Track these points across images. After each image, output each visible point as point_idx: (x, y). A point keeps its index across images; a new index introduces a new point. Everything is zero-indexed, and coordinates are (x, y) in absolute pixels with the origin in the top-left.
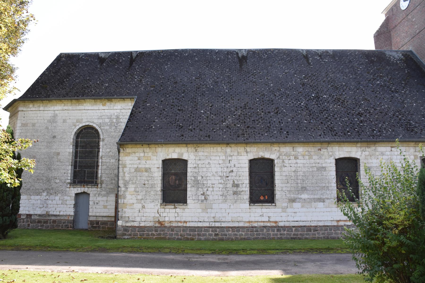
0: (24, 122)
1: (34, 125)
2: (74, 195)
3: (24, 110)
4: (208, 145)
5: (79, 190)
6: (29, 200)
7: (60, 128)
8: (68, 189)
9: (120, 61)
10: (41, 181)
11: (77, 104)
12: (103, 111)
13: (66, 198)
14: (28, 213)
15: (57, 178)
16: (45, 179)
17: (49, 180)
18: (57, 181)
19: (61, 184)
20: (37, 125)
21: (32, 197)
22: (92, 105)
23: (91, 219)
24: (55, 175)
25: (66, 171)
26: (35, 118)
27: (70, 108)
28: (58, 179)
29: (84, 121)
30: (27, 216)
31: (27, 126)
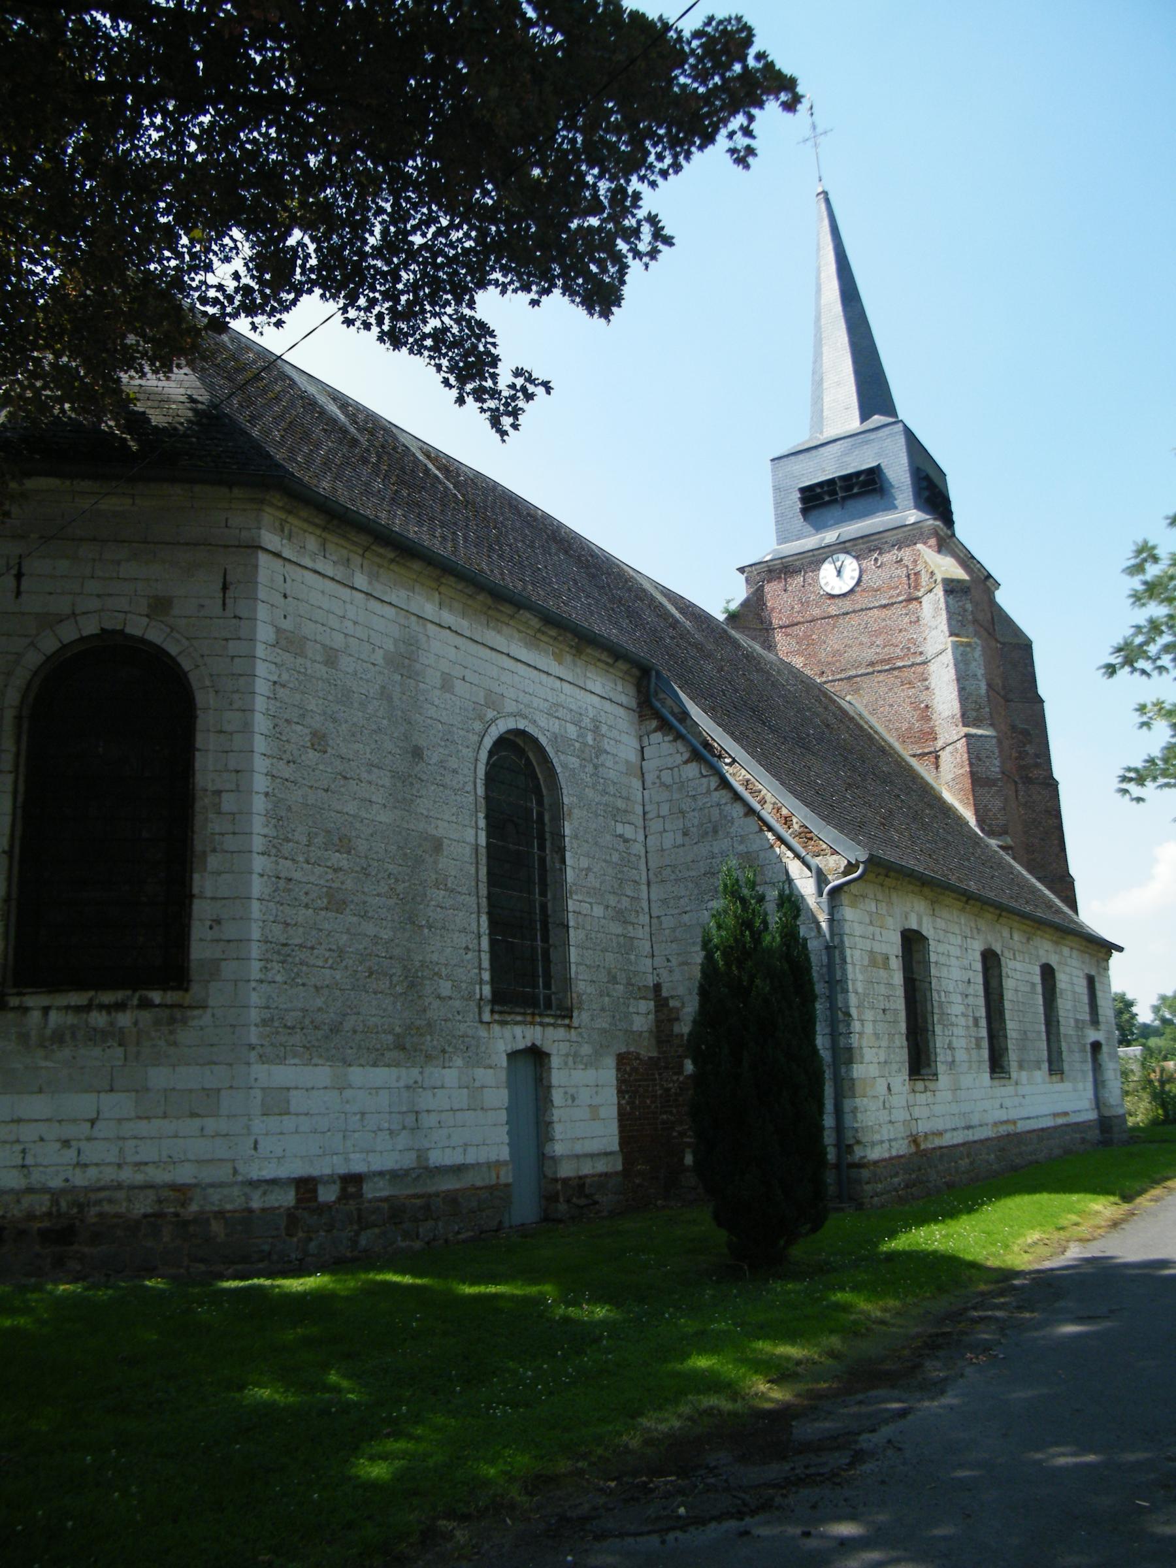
0: (286, 625)
1: (331, 658)
2: (504, 1061)
3: (285, 554)
4: (204, 883)
5: (522, 1035)
6: (341, 1089)
7: (432, 712)
8: (483, 1033)
9: (284, 295)
10: (384, 984)
11: (483, 619)
12: (558, 682)
13: (479, 1072)
14: (342, 1170)
15: (444, 972)
16: (397, 970)
17: (413, 983)
18: (446, 988)
19: (457, 1004)
20: (345, 662)
21: (356, 1074)
22: (559, 658)
23: (566, 1171)
24: (435, 957)
25: (460, 941)
26: (334, 622)
27: (463, 624)
28: (448, 977)
29: (510, 707)
30: (343, 1190)
31: (301, 653)
